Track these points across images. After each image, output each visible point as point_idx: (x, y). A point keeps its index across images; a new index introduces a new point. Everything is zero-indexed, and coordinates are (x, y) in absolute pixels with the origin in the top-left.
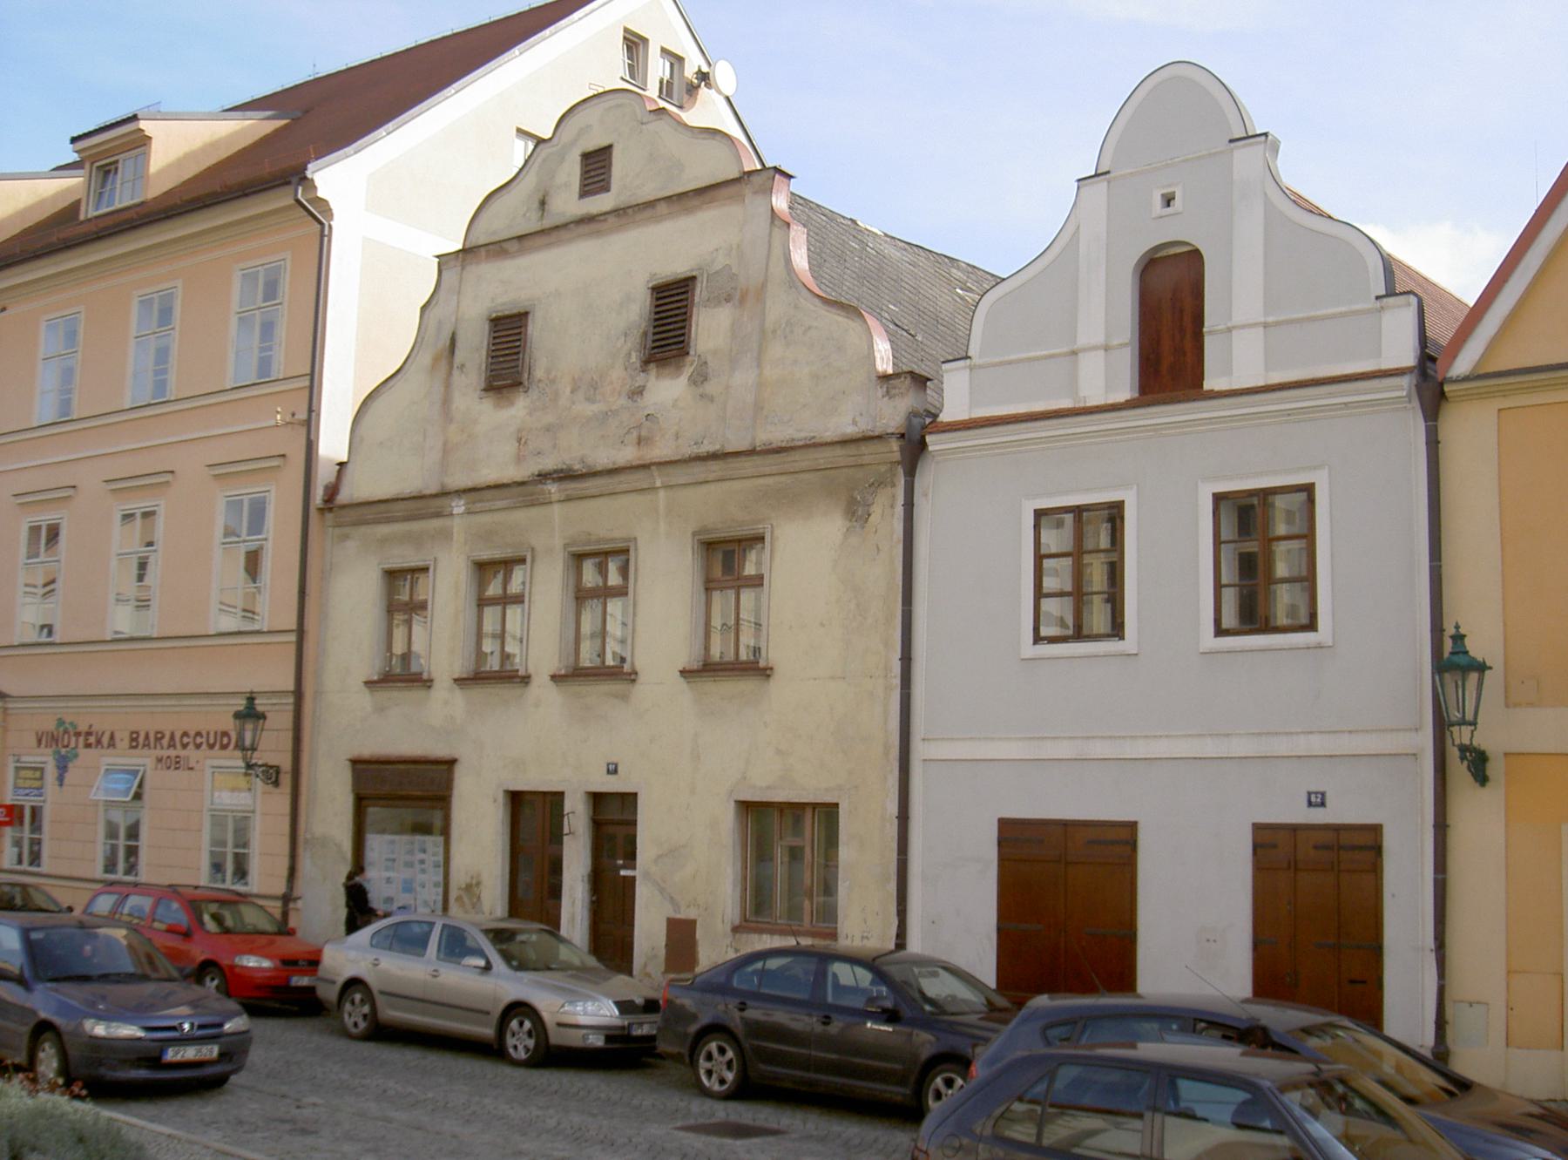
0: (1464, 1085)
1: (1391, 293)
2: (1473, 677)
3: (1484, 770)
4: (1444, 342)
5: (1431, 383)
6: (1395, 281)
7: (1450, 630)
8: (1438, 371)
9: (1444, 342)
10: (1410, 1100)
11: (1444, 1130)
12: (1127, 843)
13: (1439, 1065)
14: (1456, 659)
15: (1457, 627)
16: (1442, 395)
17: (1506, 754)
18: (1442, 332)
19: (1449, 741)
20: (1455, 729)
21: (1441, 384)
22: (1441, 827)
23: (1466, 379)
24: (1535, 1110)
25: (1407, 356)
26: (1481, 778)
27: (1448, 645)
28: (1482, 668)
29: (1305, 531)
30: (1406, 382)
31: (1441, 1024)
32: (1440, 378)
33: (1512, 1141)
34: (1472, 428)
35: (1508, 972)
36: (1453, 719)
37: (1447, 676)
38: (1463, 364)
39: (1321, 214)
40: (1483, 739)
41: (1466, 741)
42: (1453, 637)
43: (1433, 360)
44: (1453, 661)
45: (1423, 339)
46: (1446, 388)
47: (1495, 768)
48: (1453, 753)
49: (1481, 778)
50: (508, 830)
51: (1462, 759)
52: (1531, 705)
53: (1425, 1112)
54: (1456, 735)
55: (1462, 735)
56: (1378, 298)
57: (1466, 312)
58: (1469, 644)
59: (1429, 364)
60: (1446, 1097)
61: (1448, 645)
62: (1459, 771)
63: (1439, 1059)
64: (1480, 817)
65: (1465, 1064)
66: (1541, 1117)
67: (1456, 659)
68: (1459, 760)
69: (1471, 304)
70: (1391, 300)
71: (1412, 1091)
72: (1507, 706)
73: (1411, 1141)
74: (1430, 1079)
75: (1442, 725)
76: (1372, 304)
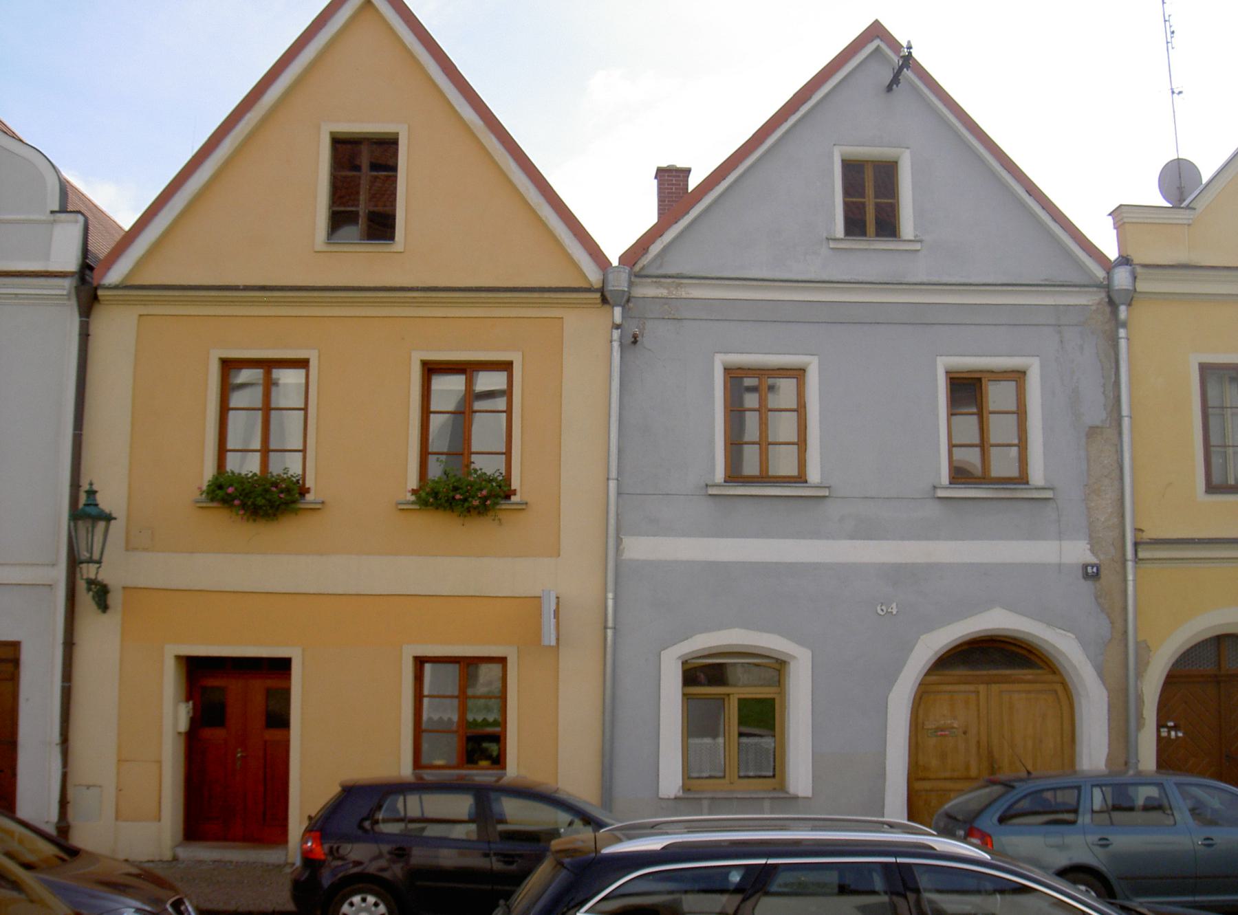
0: (74, 853)
1: (63, 210)
2: (101, 525)
3: (105, 601)
4: (101, 256)
5: (88, 287)
6: (68, 201)
7: (85, 487)
8: (94, 279)
9: (101, 256)
10: (28, 866)
11: (59, 890)
12: (10, 661)
13: (62, 841)
14: (88, 509)
15: (91, 484)
16: (95, 298)
17: (124, 588)
18: (101, 247)
19: (78, 576)
20: (84, 566)
21: (96, 289)
22: (69, 644)
23: (116, 287)
24: (135, 871)
25: (69, 261)
26: (103, 606)
27: (83, 499)
28: (109, 518)
29: (302, 406)
30: (68, 284)
31: (64, 803)
32: (95, 284)
33: (110, 896)
34: (117, 327)
35: (120, 761)
36: (83, 558)
37: (80, 523)
38: (115, 275)
39: (14, 136)
40: (105, 575)
41: (92, 576)
42: (87, 492)
43: (91, 268)
44: (86, 512)
45: (85, 251)
46: (100, 293)
47: (115, 599)
48: (81, 586)
49: (103, 606)
50: (1077, 718)
51: (89, 590)
52: (145, 550)
53: (41, 876)
54: (85, 571)
55: (89, 571)
56: (52, 212)
57: (118, 237)
58: (100, 498)
59: (88, 272)
60: (59, 862)
61: (83, 499)
62: (85, 599)
63: (61, 837)
64: (101, 635)
65: (78, 839)
66: (138, 876)
67: (88, 509)
68: (86, 590)
69: (127, 227)
70: (63, 216)
71: (30, 858)
72: (127, 550)
73: (32, 901)
74: (49, 850)
75: (74, 562)
76: (46, 216)
